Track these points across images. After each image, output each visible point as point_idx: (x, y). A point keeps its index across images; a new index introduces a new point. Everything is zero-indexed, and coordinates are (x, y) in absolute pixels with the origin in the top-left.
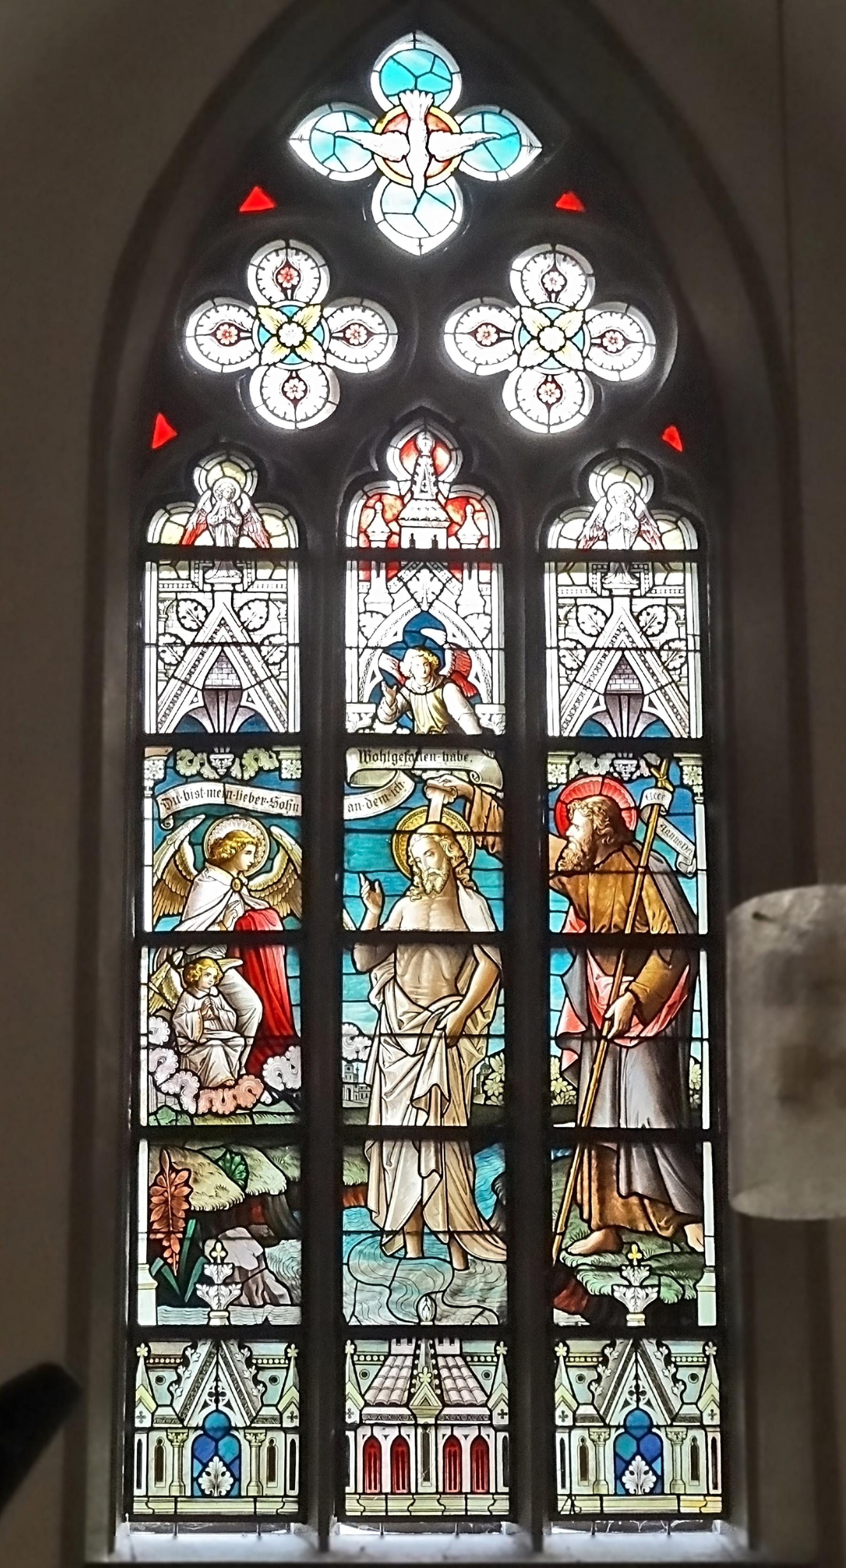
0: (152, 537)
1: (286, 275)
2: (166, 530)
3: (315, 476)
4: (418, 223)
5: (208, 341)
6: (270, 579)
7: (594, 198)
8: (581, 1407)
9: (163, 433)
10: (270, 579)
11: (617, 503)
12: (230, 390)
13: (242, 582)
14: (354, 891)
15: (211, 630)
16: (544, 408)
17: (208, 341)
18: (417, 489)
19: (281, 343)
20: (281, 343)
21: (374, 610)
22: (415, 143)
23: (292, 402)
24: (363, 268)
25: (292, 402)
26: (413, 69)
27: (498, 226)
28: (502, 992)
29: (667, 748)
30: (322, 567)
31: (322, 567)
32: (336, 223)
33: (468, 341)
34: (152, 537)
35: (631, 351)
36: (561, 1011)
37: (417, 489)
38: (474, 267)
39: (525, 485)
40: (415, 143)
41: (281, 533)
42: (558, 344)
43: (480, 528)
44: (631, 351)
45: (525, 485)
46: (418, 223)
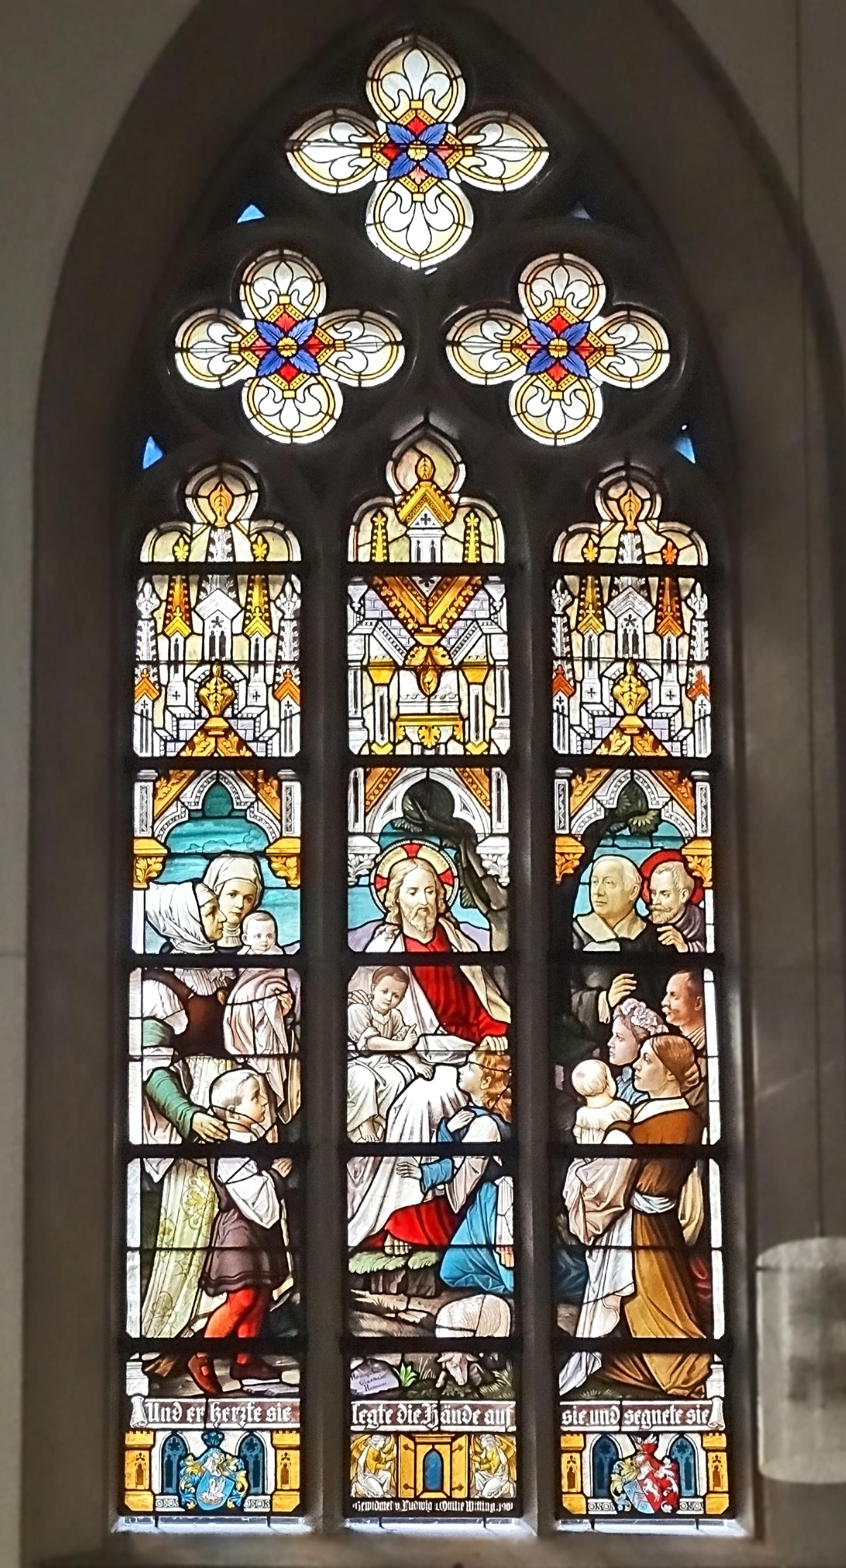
0: (145, 557)
2: (159, 549)
4: (419, 230)
8: (206, 500)
11: (631, 528)
13: (369, 875)
14: (364, 894)
16: (557, 416)
18: (427, 513)
19: (274, 357)
20: (274, 357)
22: (416, 160)
23: (294, 415)
24: (359, 281)
26: (415, 83)
28: (435, 269)
29: (684, 766)
30: (326, 585)
31: (326, 585)
32: (333, 237)
33: (480, 354)
34: (145, 557)
35: (640, 355)
37: (427, 513)
38: (485, 277)
40: (416, 160)
42: (570, 359)
43: (492, 542)
44: (640, 355)
45: (543, 494)
46: (419, 230)
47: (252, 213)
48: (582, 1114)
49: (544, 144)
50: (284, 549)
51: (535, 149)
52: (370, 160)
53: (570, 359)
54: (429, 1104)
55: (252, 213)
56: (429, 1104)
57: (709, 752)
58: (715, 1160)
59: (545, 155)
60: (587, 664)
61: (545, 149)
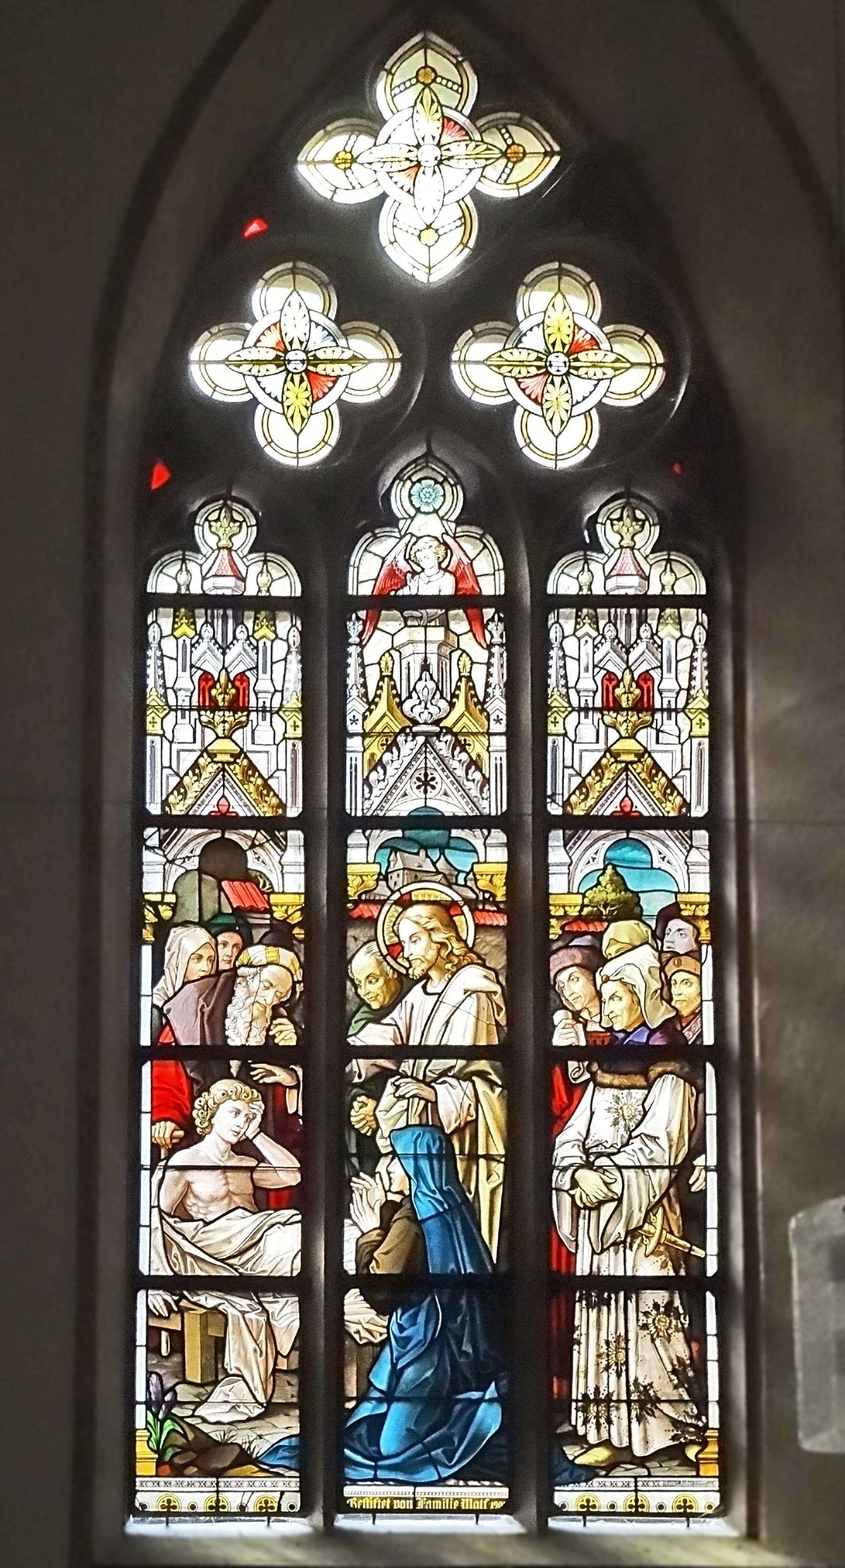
1: (288, 306)
3: (322, 517)
4: (426, 247)
5: (215, 368)
6: (243, 348)
7: (595, 222)
9: (160, 477)
10: (243, 348)
11: (625, 553)
12: (234, 423)
15: (210, 698)
16: (556, 439)
17: (215, 368)
18: (425, 531)
19: (280, 368)
20: (280, 368)
21: (579, 654)
22: (417, 163)
23: (297, 438)
24: (364, 291)
25: (297, 438)
27: (510, 246)
30: (326, 622)
31: (326, 622)
33: (478, 371)
35: (633, 372)
36: (358, 583)
37: (425, 531)
38: (484, 296)
39: (530, 514)
40: (417, 163)
41: (285, 584)
42: (566, 372)
44: (633, 372)
45: (530, 514)
46: (426, 247)
47: (254, 227)
48: (453, 502)
49: (557, 148)
50: (285, 584)
51: (546, 154)
52: (173, 714)
53: (566, 372)
54: (390, 137)
55: (254, 227)
56: (390, 137)
57: (706, 810)
58: (712, 1293)
59: (556, 159)
60: (582, 714)
61: (558, 153)
